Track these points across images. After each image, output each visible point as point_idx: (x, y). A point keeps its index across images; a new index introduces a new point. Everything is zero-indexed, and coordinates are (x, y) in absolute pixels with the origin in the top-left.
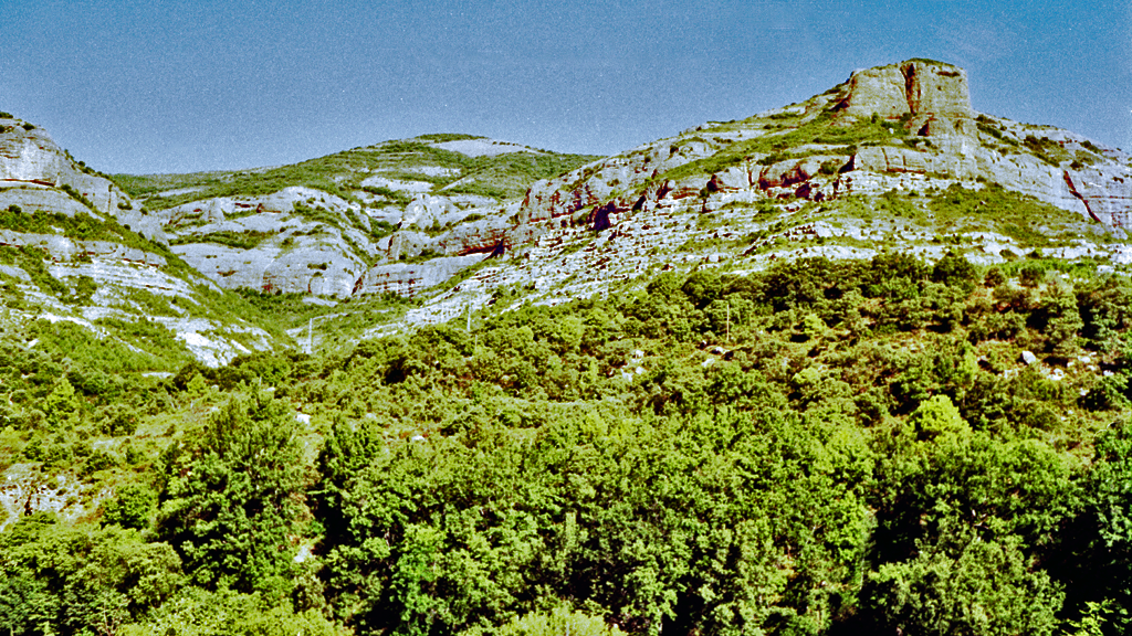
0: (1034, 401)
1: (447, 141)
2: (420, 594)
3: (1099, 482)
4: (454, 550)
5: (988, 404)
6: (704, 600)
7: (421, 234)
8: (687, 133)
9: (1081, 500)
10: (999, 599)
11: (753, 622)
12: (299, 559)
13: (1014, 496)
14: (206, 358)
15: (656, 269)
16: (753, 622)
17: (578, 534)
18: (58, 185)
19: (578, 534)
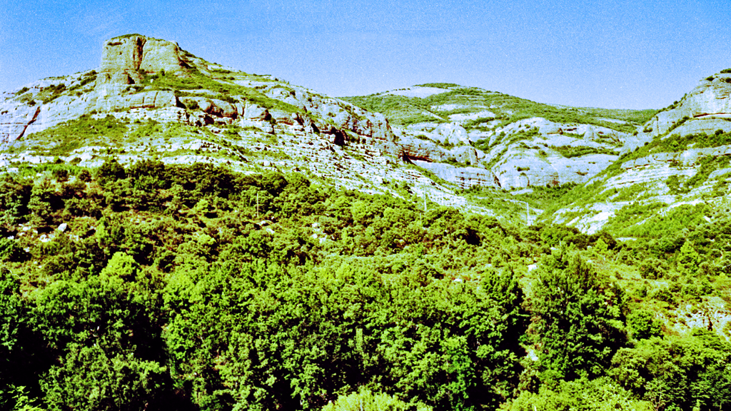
0: (339, 328)
1: (440, 88)
2: (457, 381)
3: (17, 308)
4: (42, 193)
5: (89, 258)
6: (627, 340)
7: (456, 148)
8: (284, 82)
9: (337, 353)
10: (82, 384)
11: (241, 399)
12: (19, 390)
13: (72, 318)
14: (596, 229)
15: (304, 171)
16: (241, 399)
17: (355, 342)
18: (691, 116)
19: (355, 342)
